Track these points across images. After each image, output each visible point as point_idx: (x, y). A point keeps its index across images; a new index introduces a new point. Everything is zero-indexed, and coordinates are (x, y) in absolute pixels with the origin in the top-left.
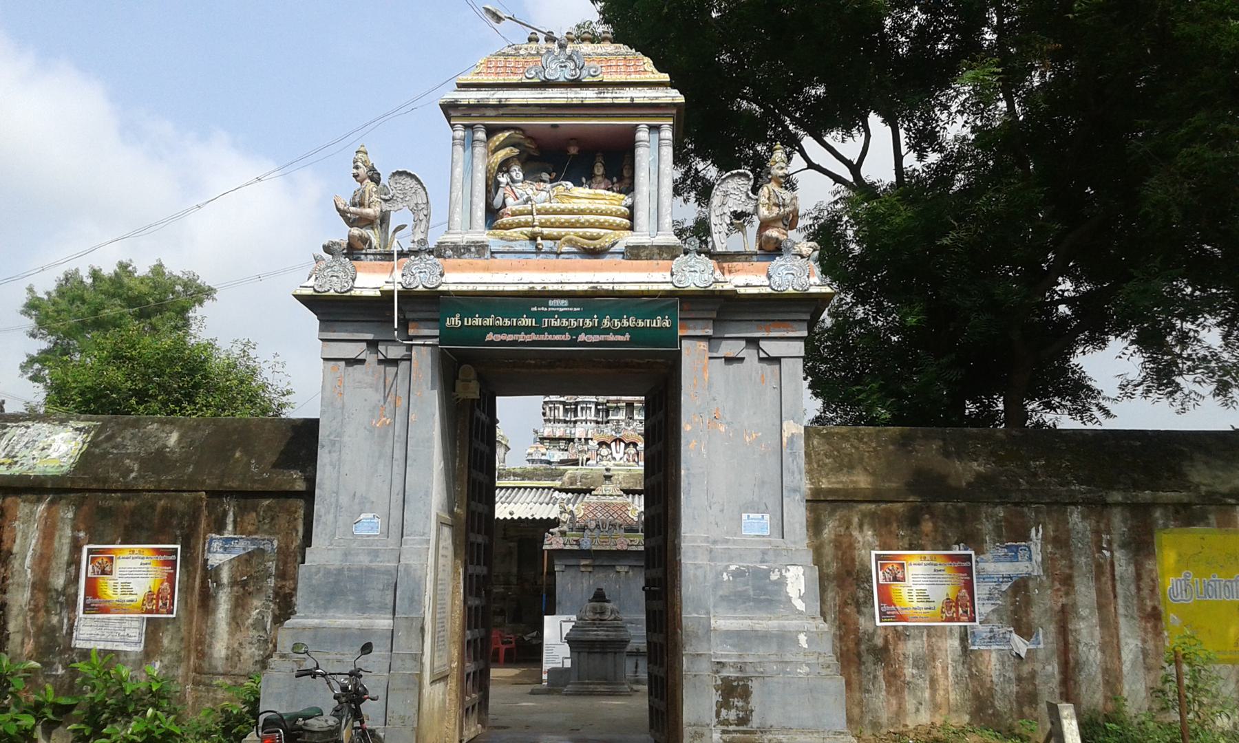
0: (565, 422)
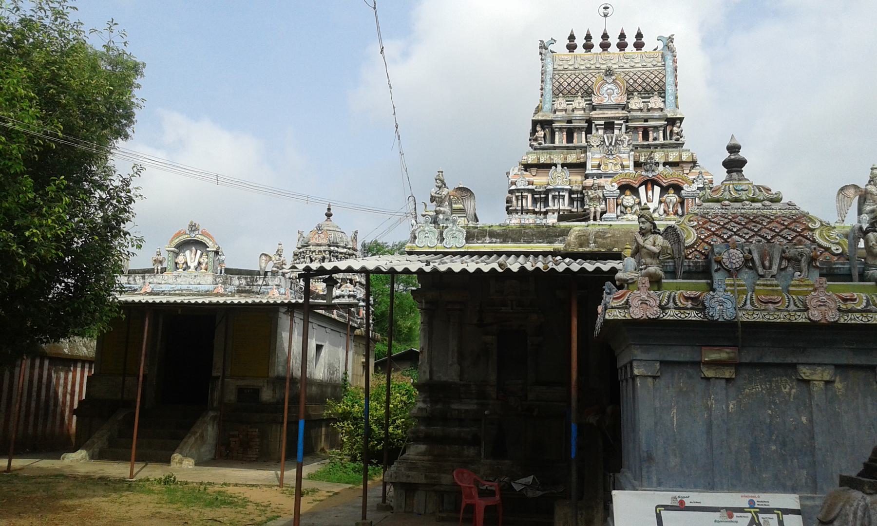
0: (534, 212)
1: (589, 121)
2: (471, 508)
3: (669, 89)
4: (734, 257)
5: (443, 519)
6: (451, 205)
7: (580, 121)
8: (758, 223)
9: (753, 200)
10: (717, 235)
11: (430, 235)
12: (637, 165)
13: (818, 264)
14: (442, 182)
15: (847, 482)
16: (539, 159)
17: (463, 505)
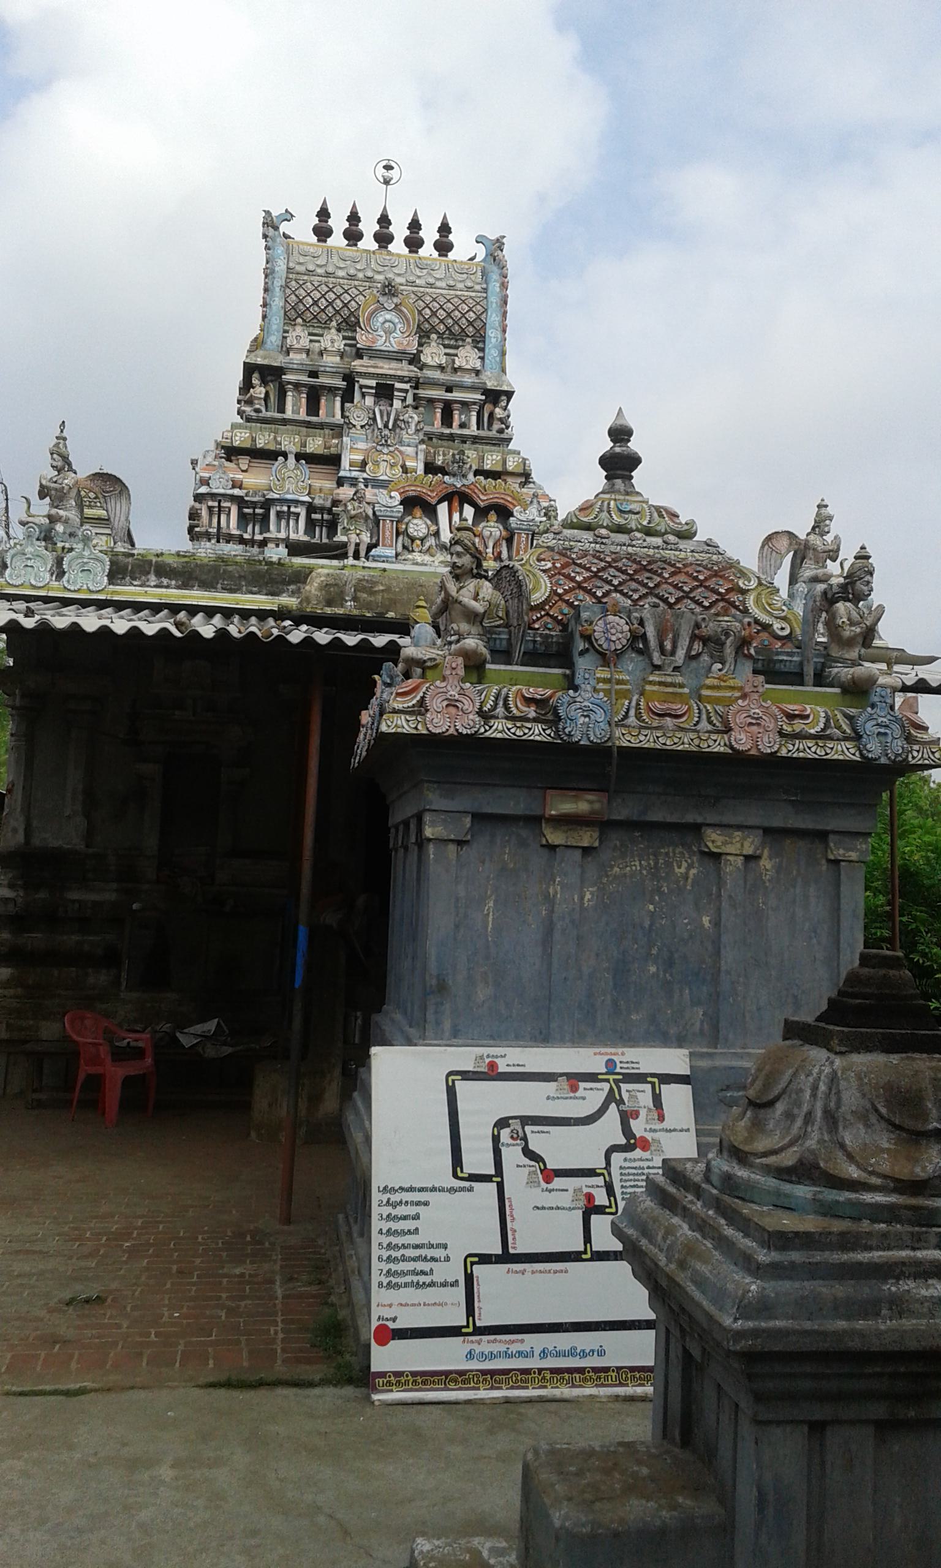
0: (242, 541)
1: (349, 378)
2: (96, 1083)
3: (492, 335)
4: (613, 630)
5: (40, 1105)
6: (80, 506)
7: (334, 374)
8: (655, 573)
9: (649, 532)
10: (585, 589)
11: (36, 563)
12: (430, 468)
13: (752, 651)
14: (65, 459)
15: (794, 1031)
16: (254, 440)
17: (81, 1077)
